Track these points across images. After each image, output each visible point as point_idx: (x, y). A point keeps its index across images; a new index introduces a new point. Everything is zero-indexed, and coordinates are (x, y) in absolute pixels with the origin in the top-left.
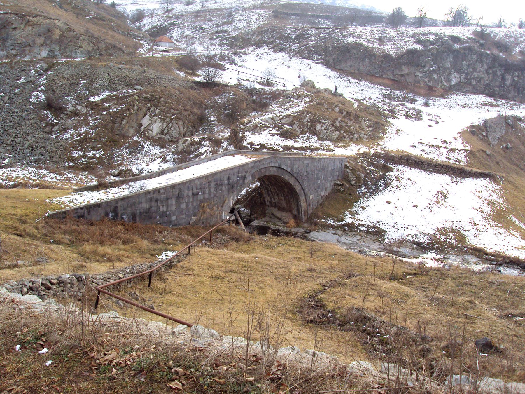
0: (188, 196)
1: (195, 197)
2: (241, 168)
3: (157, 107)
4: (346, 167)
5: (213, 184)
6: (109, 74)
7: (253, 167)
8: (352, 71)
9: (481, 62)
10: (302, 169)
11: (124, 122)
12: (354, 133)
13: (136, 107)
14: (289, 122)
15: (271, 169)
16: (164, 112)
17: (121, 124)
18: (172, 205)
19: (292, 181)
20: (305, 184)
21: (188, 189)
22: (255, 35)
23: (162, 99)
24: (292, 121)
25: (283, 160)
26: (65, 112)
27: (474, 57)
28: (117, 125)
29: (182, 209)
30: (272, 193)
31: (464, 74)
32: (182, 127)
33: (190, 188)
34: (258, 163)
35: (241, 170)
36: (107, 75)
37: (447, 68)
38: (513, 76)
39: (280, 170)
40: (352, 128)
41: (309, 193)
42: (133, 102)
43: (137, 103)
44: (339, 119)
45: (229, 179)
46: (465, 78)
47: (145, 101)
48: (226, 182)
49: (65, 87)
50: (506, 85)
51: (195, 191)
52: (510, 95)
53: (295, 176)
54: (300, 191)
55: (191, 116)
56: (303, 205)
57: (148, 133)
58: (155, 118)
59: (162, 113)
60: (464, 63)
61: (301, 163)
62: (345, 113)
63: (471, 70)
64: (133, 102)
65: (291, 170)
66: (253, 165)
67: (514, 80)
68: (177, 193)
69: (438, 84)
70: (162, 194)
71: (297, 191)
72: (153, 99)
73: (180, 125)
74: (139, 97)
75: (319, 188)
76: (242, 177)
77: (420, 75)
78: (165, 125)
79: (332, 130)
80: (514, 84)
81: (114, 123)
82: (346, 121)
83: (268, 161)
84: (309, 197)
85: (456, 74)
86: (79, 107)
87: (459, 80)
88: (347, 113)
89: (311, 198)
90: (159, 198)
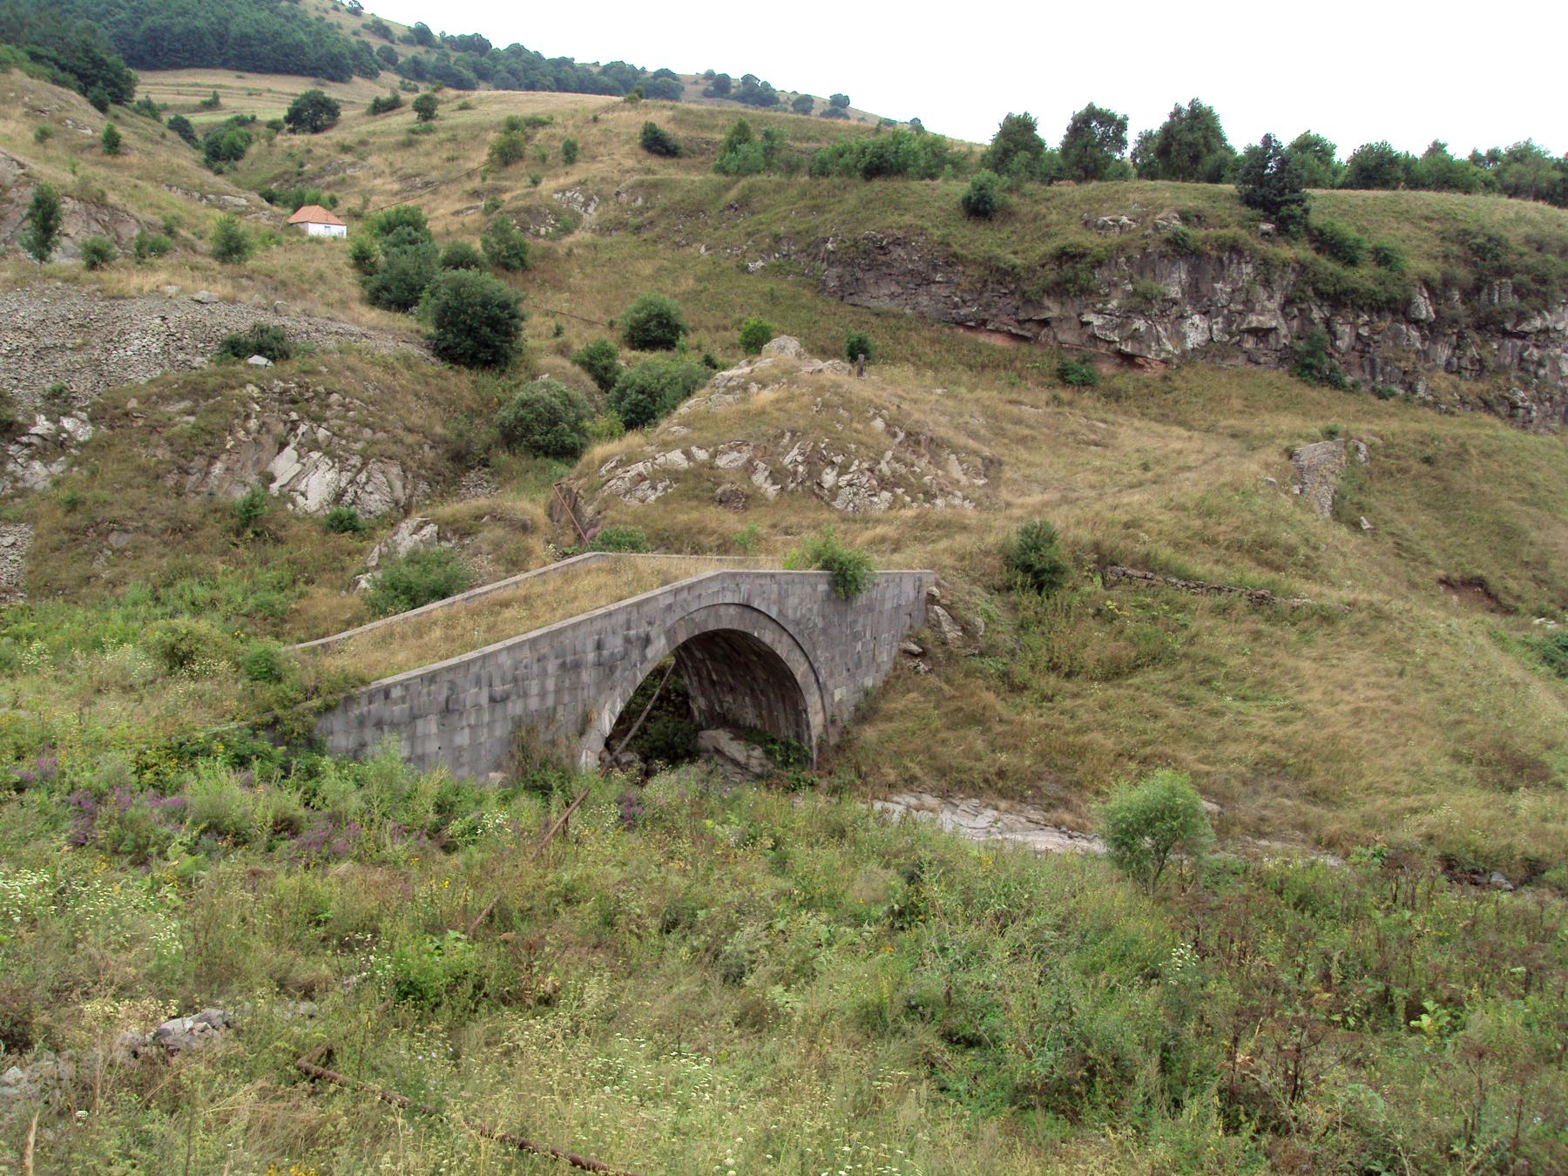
0: (477, 706)
1: (499, 707)
2: (635, 612)
3: (318, 420)
4: (932, 600)
5: (552, 667)
6: (164, 319)
7: (669, 608)
8: (896, 310)
9: (1267, 283)
10: (810, 610)
11: (218, 469)
12: (935, 497)
13: (253, 424)
14: (740, 463)
15: (722, 610)
16: (342, 437)
17: (207, 473)
18: (426, 736)
19: (783, 649)
20: (821, 655)
21: (478, 682)
22: (593, 205)
23: (335, 397)
24: (750, 461)
25: (758, 581)
26: (24, 439)
27: (1248, 269)
28: (193, 478)
29: (460, 749)
30: (713, 683)
31: (1220, 319)
32: (398, 484)
33: (484, 681)
34: (684, 595)
35: (635, 616)
36: (158, 321)
37: (1175, 302)
38: (1354, 325)
39: (748, 615)
40: (927, 479)
41: (830, 684)
42: (244, 405)
43: (258, 408)
44: (889, 454)
45: (599, 646)
46: (1224, 331)
47: (281, 402)
48: (591, 657)
49: (20, 359)
50: (1337, 350)
51: (499, 689)
52: (1348, 379)
53: (791, 629)
54: (804, 675)
55: (426, 448)
56: (816, 720)
57: (294, 503)
58: (315, 455)
59: (336, 439)
60: (1218, 286)
61: (808, 589)
62: (901, 435)
63: (1240, 307)
64: (244, 405)
65: (780, 612)
66: (670, 600)
67: (1359, 337)
68: (442, 698)
69: (1149, 347)
70: (395, 703)
71: (798, 678)
72: (307, 395)
73: (392, 477)
74: (263, 390)
75: (858, 665)
76: (638, 638)
77: (1096, 321)
78: (346, 476)
79: (872, 488)
80: (1359, 347)
81: (185, 472)
82: (909, 457)
83: (715, 587)
84: (832, 695)
85: (1196, 318)
86: (67, 423)
87: (1207, 336)
88: (909, 434)
89: (837, 699)
90: (387, 715)
